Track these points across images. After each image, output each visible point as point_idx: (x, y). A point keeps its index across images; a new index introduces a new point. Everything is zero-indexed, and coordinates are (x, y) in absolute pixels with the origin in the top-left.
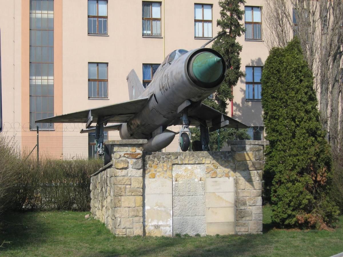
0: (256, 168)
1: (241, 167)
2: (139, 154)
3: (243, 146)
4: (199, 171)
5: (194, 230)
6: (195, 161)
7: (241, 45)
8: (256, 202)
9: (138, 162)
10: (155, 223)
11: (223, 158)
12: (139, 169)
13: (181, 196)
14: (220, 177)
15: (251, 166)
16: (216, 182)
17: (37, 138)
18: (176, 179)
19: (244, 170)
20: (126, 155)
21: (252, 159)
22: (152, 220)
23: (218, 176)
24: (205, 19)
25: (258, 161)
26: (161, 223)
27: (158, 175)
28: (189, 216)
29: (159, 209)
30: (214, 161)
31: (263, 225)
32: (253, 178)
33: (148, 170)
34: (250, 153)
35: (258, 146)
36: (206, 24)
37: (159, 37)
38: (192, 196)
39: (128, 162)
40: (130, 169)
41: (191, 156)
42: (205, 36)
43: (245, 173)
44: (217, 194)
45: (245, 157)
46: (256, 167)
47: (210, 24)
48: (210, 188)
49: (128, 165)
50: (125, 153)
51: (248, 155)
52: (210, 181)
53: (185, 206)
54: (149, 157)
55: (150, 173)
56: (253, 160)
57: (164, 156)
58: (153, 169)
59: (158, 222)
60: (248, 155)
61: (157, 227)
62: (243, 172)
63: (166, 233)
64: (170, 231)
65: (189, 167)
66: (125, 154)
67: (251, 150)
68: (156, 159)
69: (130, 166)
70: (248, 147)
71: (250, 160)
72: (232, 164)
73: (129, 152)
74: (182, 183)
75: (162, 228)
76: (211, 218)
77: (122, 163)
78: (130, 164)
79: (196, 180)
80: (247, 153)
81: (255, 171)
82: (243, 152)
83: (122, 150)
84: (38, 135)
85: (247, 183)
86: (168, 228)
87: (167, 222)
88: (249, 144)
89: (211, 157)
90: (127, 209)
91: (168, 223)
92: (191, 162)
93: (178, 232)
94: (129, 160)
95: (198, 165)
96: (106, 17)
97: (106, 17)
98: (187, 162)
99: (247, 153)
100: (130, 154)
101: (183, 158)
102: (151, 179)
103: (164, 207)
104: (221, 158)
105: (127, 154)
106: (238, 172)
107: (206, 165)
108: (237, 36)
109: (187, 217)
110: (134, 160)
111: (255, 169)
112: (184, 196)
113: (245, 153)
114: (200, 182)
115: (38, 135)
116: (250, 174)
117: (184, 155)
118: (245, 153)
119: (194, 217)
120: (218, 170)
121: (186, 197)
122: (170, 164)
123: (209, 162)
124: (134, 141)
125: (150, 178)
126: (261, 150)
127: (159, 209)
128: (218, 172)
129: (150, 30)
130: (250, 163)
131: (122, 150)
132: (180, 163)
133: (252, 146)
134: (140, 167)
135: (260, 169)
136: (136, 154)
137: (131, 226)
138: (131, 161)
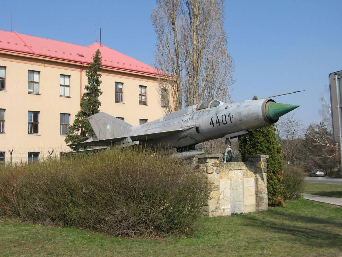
1: (257, 170)
4: (240, 173)
7: (100, 102)
9: (218, 169)
10: (223, 208)
13: (233, 190)
16: (247, 180)
17: (10, 158)
19: (260, 173)
20: (213, 165)
24: (65, 84)
26: (226, 207)
27: (224, 177)
32: (264, 177)
34: (263, 163)
36: (66, 88)
37: (38, 94)
40: (214, 173)
42: (65, 95)
46: (265, 171)
47: (68, 88)
57: (226, 165)
62: (260, 174)
65: (236, 171)
66: (212, 164)
68: (222, 167)
70: (262, 159)
71: (263, 167)
72: (253, 170)
77: (211, 170)
79: (239, 180)
83: (211, 161)
84: (11, 156)
85: (262, 181)
86: (229, 210)
89: (245, 165)
93: (233, 213)
94: (214, 167)
95: (240, 171)
96: (4, 79)
97: (4, 79)
100: (215, 164)
104: (249, 166)
105: (213, 164)
106: (258, 174)
109: (236, 203)
115: (11, 156)
116: (262, 175)
117: (234, 164)
120: (248, 173)
122: (228, 170)
129: (32, 89)
130: (263, 169)
131: (211, 161)
136: (217, 164)
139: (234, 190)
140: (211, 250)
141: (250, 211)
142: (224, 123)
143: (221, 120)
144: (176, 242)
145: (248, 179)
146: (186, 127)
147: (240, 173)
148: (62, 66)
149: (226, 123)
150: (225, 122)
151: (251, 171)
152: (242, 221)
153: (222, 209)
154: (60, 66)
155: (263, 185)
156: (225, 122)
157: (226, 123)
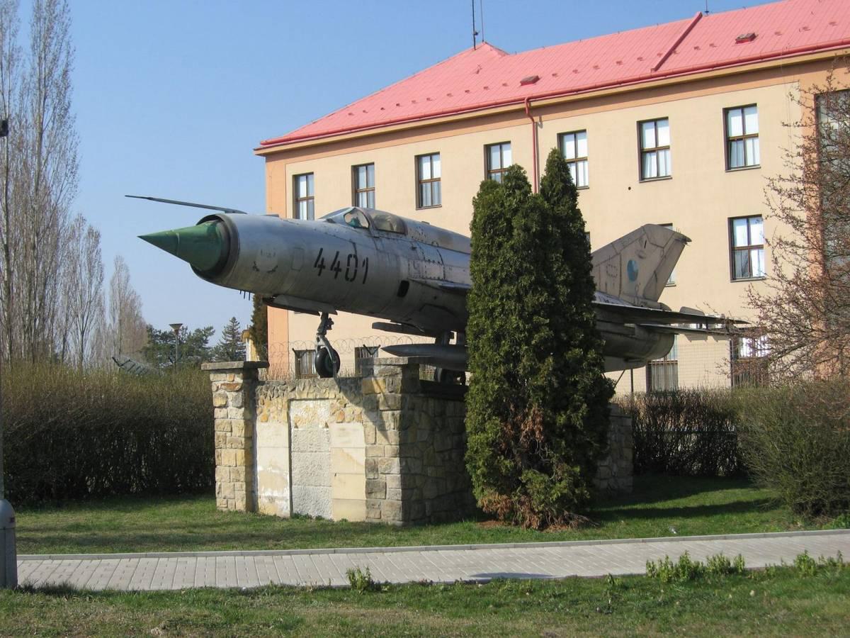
0: (388, 406)
2: (238, 384)
3: (369, 367)
5: (318, 510)
6: (316, 395)
8: (390, 467)
10: (268, 493)
11: (353, 390)
12: (240, 408)
14: (349, 422)
15: (383, 403)
16: (343, 429)
18: (296, 424)
21: (384, 391)
22: (266, 489)
23: (346, 420)
25: (393, 393)
26: (276, 494)
28: (312, 485)
29: (273, 471)
30: (341, 395)
31: (214, 498)
33: (260, 409)
35: (392, 367)
38: (316, 452)
39: (227, 397)
41: (312, 386)
42: (661, 175)
43: (374, 414)
44: (346, 451)
45: (372, 386)
48: (337, 441)
49: (226, 402)
50: (223, 382)
51: (377, 383)
52: (335, 427)
53: (307, 467)
54: (261, 389)
55: (262, 414)
56: (386, 392)
58: (265, 408)
59: (272, 493)
60: (377, 383)
61: (272, 499)
63: (282, 510)
64: (287, 508)
65: (311, 404)
67: (381, 373)
69: (230, 403)
73: (226, 382)
74: (302, 431)
75: (277, 501)
76: (338, 492)
78: (229, 400)
79: (320, 426)
80: (376, 380)
81: (390, 412)
82: (369, 378)
87: (283, 492)
88: (378, 363)
90: (227, 469)
91: (284, 496)
92: (311, 396)
98: (305, 397)
99: (376, 380)
101: (302, 390)
102: (263, 424)
103: (280, 469)
104: (351, 389)
107: (331, 402)
108: (557, 148)
110: (235, 394)
111: (387, 408)
112: (305, 452)
113: (373, 379)
114: (325, 429)
116: (381, 417)
118: (373, 379)
119: (318, 487)
121: (308, 454)
123: (334, 397)
124: (228, 365)
125: (262, 422)
126: (397, 374)
127: (273, 471)
128: (346, 414)
130: (381, 398)
132: (298, 398)
133: (382, 367)
134: (240, 405)
135: (395, 408)
137: (232, 496)
138: (231, 395)
139: (304, 454)
140: (827, 634)
141: (347, 519)
142: (349, 276)
143: (343, 266)
144: (804, 586)
145: (344, 425)
146: (434, 279)
147: (323, 410)
148: (413, 136)
149: (352, 280)
150: (351, 275)
151: (357, 404)
152: (127, 535)
153: (265, 497)
154: (424, 134)
155: (388, 446)
156: (351, 275)
157: (352, 280)
